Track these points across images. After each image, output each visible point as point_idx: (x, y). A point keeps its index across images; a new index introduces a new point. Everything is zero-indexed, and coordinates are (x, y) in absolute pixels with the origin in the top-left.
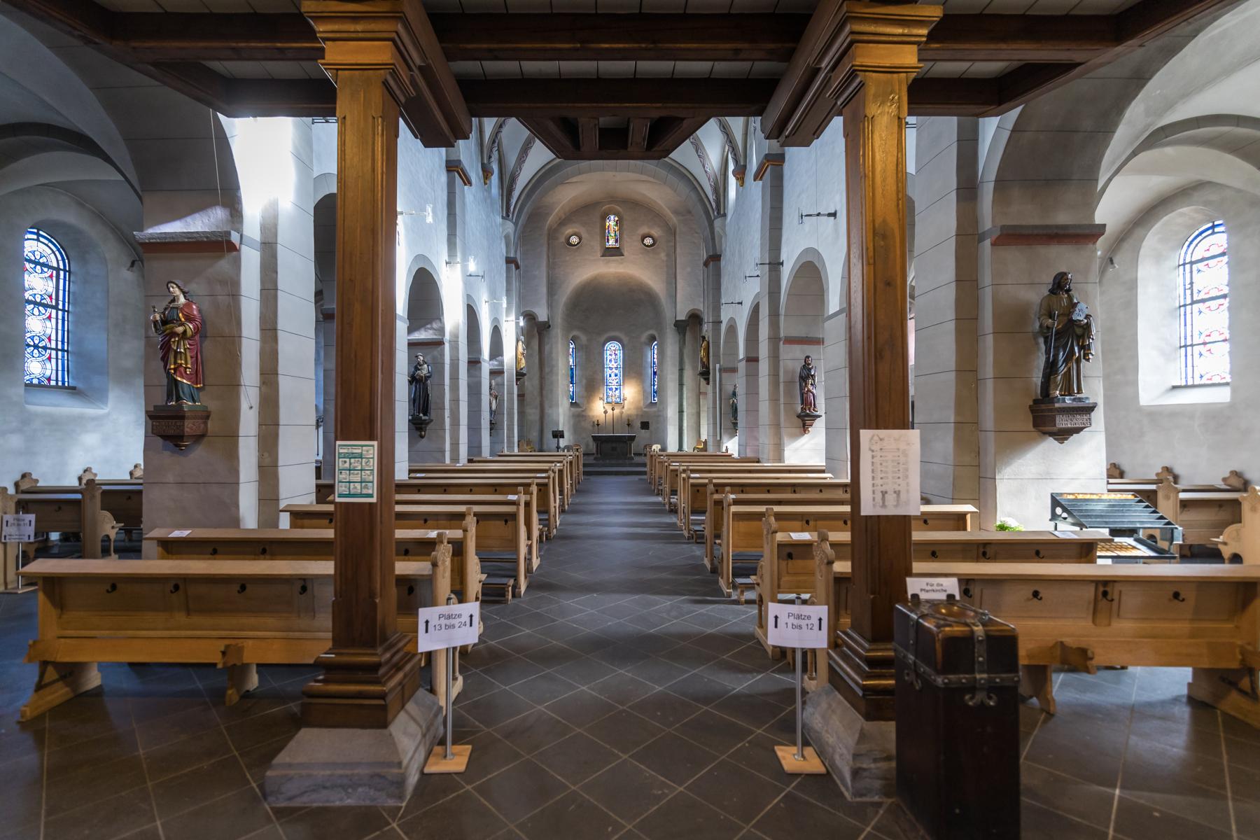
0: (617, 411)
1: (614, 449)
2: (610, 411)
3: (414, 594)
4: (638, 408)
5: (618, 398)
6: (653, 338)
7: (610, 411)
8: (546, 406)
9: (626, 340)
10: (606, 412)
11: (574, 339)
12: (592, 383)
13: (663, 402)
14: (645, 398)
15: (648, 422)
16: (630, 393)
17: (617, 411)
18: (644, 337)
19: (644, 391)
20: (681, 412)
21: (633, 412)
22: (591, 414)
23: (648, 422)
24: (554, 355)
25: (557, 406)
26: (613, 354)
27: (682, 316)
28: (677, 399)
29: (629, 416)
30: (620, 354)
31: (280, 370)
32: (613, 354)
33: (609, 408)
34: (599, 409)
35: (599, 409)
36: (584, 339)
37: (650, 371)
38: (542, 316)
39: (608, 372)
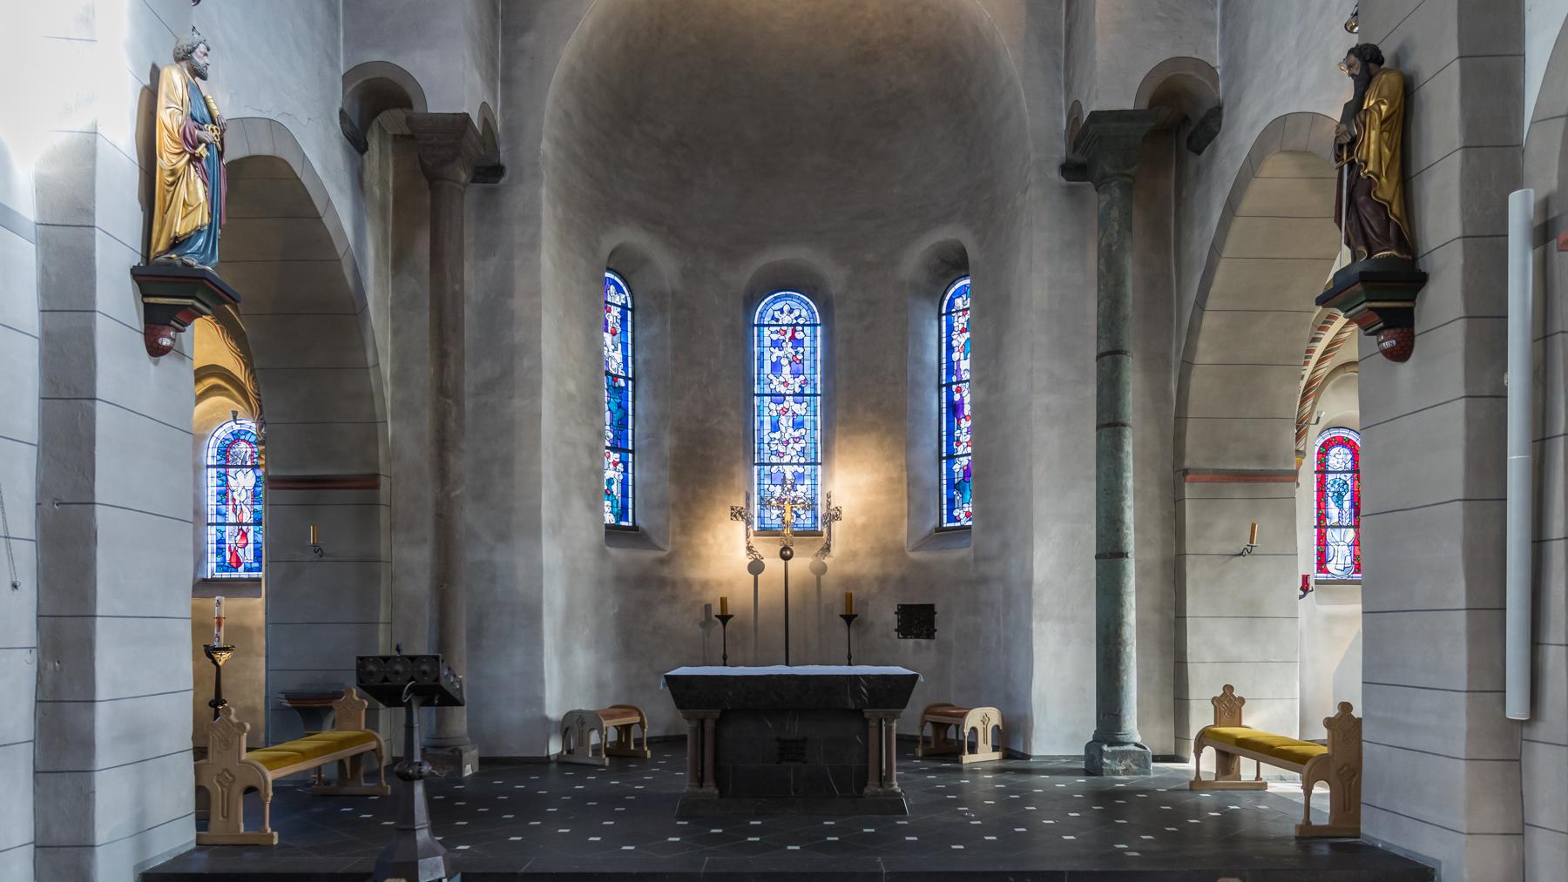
0: (801, 563)
1: (791, 750)
2: (773, 564)
3: (959, 443)
4: (886, 551)
5: (804, 512)
6: (953, 264)
7: (773, 564)
8: (469, 516)
9: (835, 276)
10: (756, 568)
11: (625, 266)
12: (700, 448)
13: (1003, 519)
14: (916, 509)
15: (934, 604)
16: (856, 490)
17: (801, 563)
18: (914, 259)
19: (913, 482)
20: (1110, 555)
21: (868, 567)
22: (697, 574)
23: (934, 604)
24: (519, 303)
25: (534, 531)
26: (787, 344)
27: (1114, 87)
28: (1085, 498)
29: (849, 582)
30: (813, 341)
31: (102, 491)
32: (787, 344)
33: (769, 552)
34: (729, 554)
35: (729, 554)
36: (666, 265)
37: (933, 402)
38: (452, 82)
39: (769, 409)
